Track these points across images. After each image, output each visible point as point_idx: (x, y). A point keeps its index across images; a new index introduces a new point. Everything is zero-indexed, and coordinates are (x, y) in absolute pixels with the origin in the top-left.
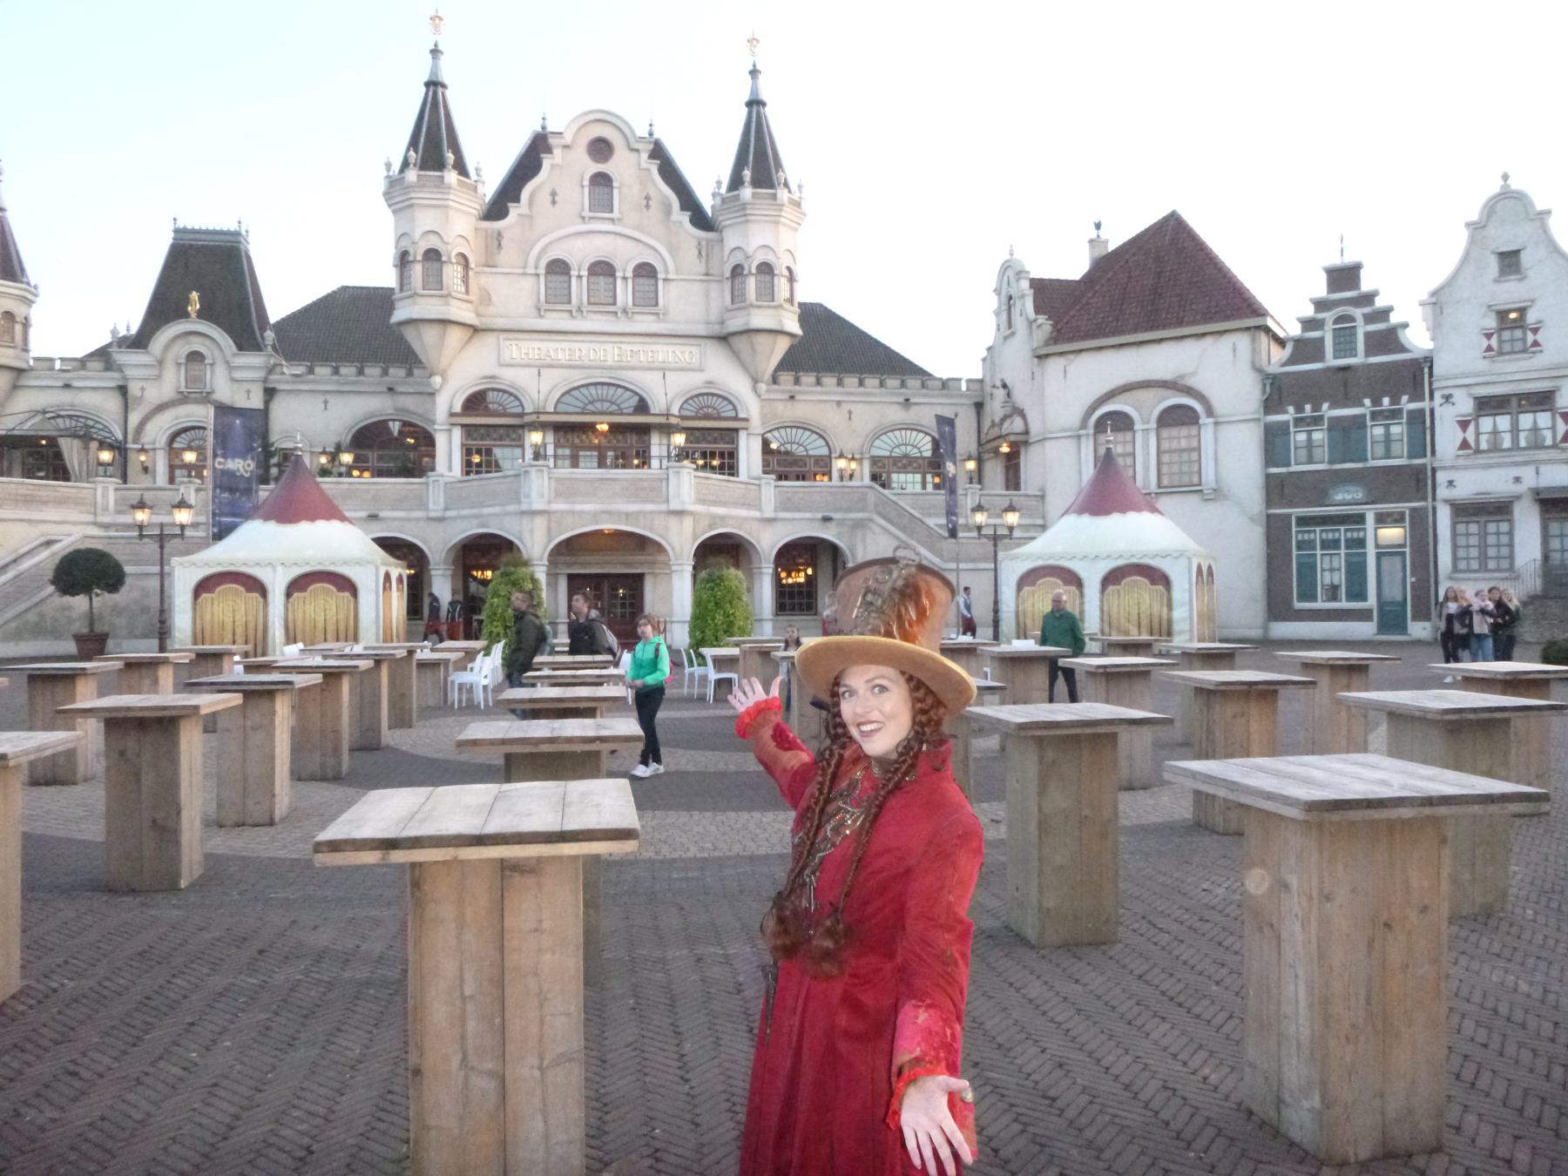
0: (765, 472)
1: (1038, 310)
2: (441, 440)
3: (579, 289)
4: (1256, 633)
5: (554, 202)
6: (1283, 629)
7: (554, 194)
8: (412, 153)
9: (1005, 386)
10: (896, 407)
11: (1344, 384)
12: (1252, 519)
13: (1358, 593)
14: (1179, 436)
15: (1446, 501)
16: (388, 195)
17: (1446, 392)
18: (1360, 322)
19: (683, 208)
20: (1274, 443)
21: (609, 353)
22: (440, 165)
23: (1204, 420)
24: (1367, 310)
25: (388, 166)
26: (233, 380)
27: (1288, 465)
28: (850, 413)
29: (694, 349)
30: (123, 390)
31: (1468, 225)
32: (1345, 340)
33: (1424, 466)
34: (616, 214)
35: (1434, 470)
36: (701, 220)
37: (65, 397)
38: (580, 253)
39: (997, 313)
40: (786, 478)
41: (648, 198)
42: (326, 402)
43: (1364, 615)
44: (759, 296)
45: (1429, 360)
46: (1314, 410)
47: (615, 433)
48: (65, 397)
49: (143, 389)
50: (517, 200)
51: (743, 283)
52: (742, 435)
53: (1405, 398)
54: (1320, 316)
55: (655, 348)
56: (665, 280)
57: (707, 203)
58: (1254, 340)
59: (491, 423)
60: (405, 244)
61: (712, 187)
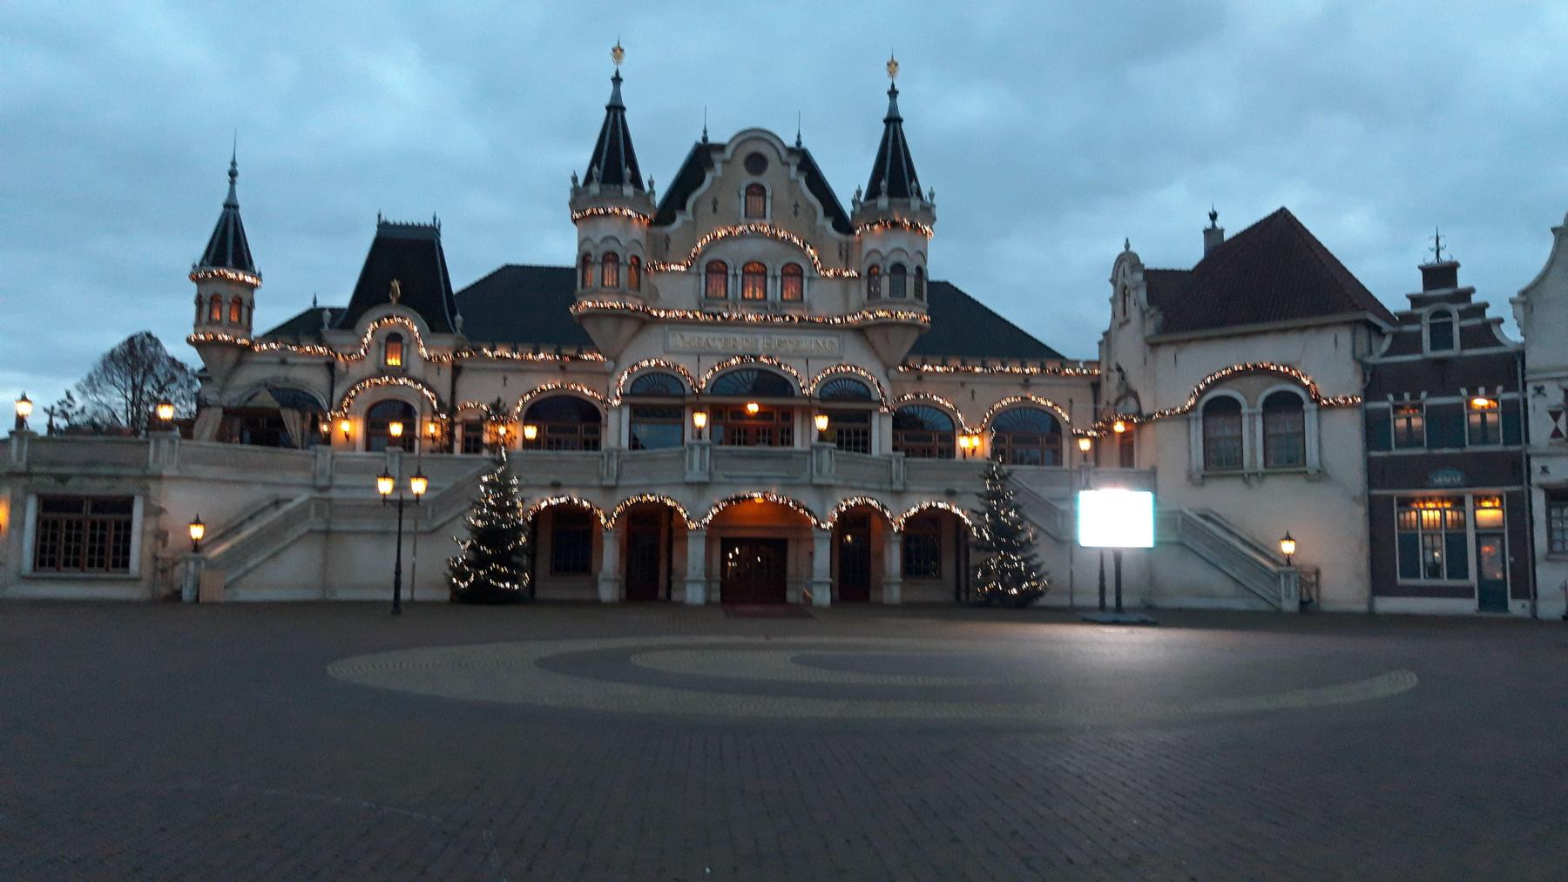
0: (895, 449)
1: (1151, 300)
2: (612, 419)
4: (1362, 607)
5: (715, 210)
6: (1387, 605)
7: (715, 203)
8: (595, 169)
9: (1119, 369)
11: (1444, 376)
12: (1354, 499)
13: (1458, 569)
14: (1285, 423)
15: (1541, 486)
16: (574, 205)
17: (1538, 384)
18: (1456, 316)
19: (827, 214)
20: (1375, 431)
21: (760, 343)
22: (619, 180)
23: (1307, 405)
24: (1462, 306)
25: (575, 179)
29: (835, 340)
30: (331, 366)
31: (1554, 230)
32: (1441, 336)
33: (1520, 452)
35: (1528, 458)
36: (843, 224)
37: (281, 372)
39: (1113, 301)
41: (796, 206)
43: (1466, 593)
44: (892, 292)
45: (1519, 355)
46: (1412, 398)
47: (757, 412)
48: (281, 372)
50: (683, 207)
53: (1500, 389)
54: (1417, 311)
55: (799, 338)
57: (848, 208)
58: (1354, 333)
59: (658, 402)
60: (588, 247)
61: (852, 195)
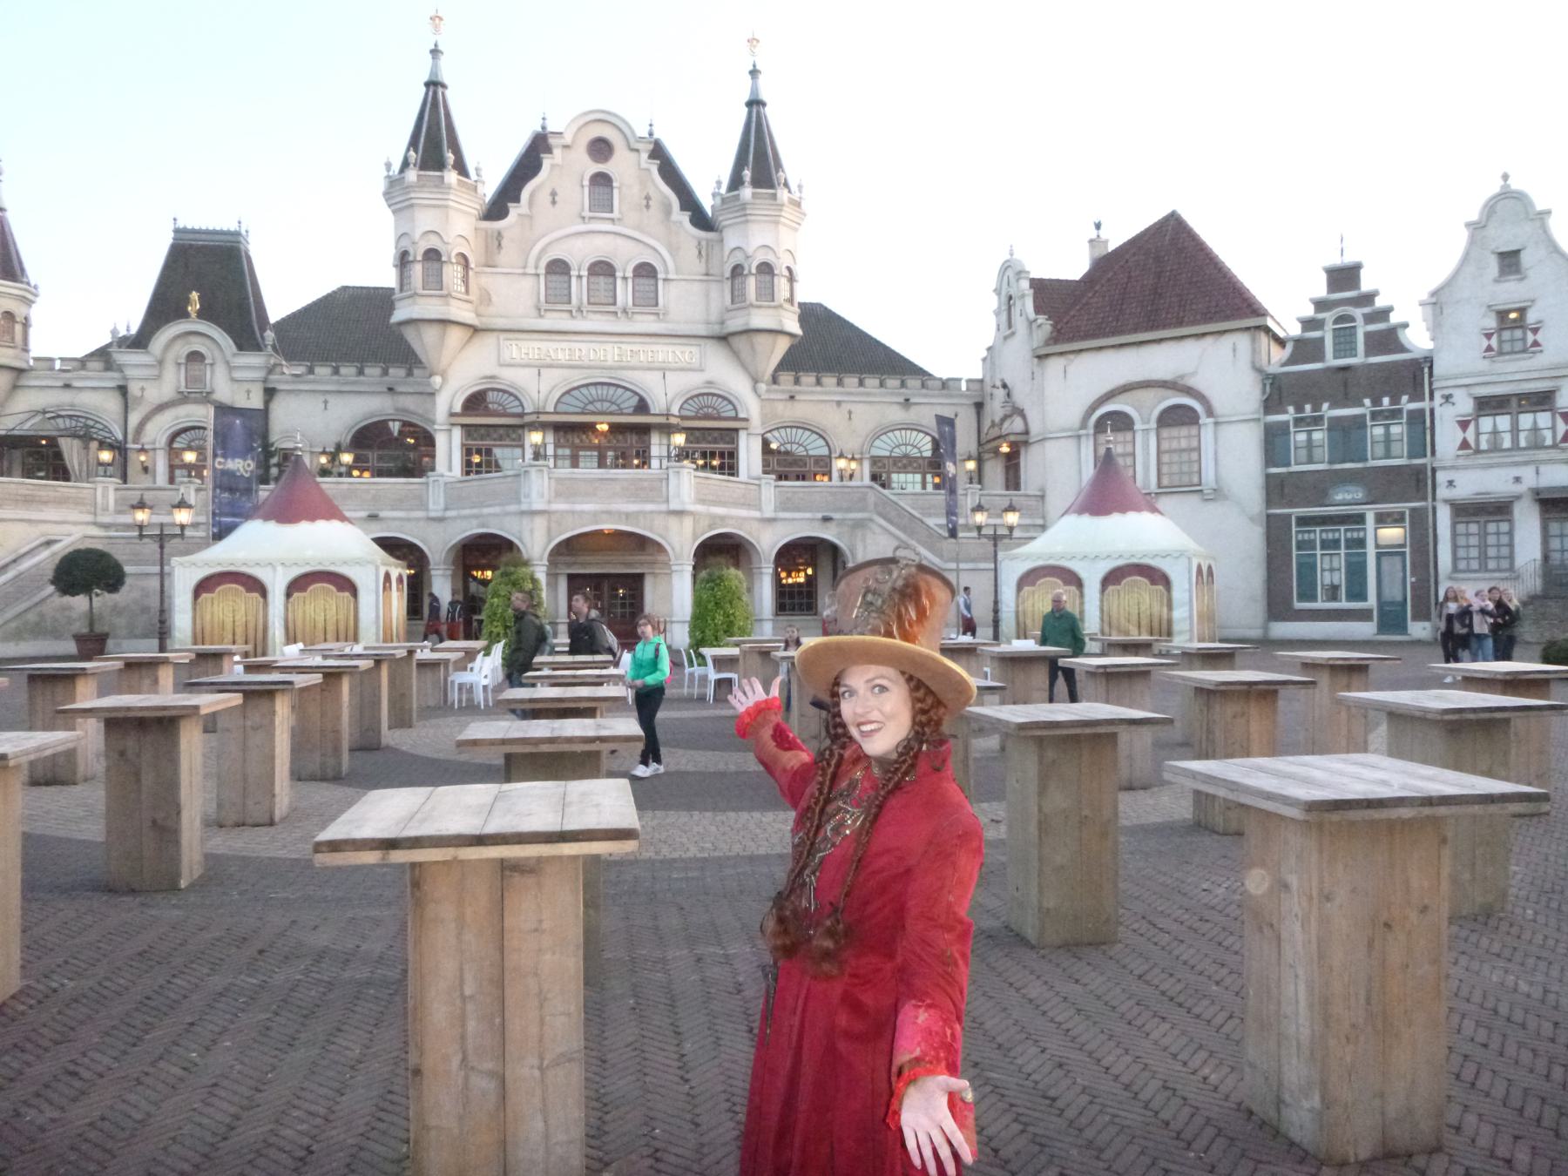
0: (765, 472)
1: (1038, 310)
2: (441, 440)
3: (579, 289)
4: (1256, 633)
5: (554, 202)
6: (1283, 629)
7: (554, 194)
8: (412, 153)
9: (1005, 386)
10: (896, 407)
11: (1344, 384)
12: (1252, 519)
13: (1358, 593)
14: (1179, 436)
15: (1446, 501)
16: (388, 195)
17: (1446, 392)
18: (1360, 322)
19: (683, 208)
20: (1274, 443)
21: (609, 353)
22: (440, 165)
23: (1204, 420)
24: (1367, 310)
25: (388, 166)
26: (233, 380)
27: (1288, 465)
28: (850, 413)
29: (694, 349)
30: (123, 390)
31: (1468, 225)
32: (1345, 340)
33: (1424, 466)
34: (616, 214)
35: (1434, 470)
36: (701, 220)
37: (65, 397)
38: (580, 253)
39: (997, 313)
40: (786, 478)
41: (648, 198)
42: (326, 402)
43: (1364, 615)
44: (759, 296)
45: (1429, 360)
46: (1314, 410)
48: (65, 397)
49: (143, 389)
50: (517, 200)
51: (743, 283)
52: (742, 435)
53: (1405, 398)
54: (1320, 316)
55: (655, 348)
56: (665, 280)
57: (707, 203)
58: (1254, 340)
59: (491, 423)
60: (405, 244)
61: (712, 187)
